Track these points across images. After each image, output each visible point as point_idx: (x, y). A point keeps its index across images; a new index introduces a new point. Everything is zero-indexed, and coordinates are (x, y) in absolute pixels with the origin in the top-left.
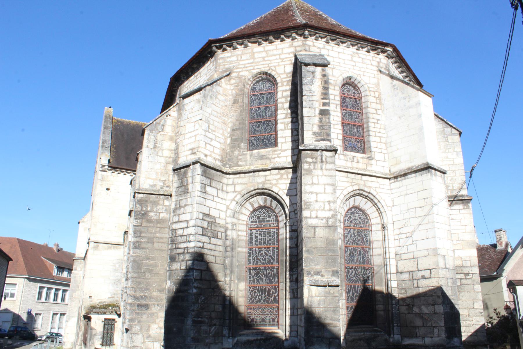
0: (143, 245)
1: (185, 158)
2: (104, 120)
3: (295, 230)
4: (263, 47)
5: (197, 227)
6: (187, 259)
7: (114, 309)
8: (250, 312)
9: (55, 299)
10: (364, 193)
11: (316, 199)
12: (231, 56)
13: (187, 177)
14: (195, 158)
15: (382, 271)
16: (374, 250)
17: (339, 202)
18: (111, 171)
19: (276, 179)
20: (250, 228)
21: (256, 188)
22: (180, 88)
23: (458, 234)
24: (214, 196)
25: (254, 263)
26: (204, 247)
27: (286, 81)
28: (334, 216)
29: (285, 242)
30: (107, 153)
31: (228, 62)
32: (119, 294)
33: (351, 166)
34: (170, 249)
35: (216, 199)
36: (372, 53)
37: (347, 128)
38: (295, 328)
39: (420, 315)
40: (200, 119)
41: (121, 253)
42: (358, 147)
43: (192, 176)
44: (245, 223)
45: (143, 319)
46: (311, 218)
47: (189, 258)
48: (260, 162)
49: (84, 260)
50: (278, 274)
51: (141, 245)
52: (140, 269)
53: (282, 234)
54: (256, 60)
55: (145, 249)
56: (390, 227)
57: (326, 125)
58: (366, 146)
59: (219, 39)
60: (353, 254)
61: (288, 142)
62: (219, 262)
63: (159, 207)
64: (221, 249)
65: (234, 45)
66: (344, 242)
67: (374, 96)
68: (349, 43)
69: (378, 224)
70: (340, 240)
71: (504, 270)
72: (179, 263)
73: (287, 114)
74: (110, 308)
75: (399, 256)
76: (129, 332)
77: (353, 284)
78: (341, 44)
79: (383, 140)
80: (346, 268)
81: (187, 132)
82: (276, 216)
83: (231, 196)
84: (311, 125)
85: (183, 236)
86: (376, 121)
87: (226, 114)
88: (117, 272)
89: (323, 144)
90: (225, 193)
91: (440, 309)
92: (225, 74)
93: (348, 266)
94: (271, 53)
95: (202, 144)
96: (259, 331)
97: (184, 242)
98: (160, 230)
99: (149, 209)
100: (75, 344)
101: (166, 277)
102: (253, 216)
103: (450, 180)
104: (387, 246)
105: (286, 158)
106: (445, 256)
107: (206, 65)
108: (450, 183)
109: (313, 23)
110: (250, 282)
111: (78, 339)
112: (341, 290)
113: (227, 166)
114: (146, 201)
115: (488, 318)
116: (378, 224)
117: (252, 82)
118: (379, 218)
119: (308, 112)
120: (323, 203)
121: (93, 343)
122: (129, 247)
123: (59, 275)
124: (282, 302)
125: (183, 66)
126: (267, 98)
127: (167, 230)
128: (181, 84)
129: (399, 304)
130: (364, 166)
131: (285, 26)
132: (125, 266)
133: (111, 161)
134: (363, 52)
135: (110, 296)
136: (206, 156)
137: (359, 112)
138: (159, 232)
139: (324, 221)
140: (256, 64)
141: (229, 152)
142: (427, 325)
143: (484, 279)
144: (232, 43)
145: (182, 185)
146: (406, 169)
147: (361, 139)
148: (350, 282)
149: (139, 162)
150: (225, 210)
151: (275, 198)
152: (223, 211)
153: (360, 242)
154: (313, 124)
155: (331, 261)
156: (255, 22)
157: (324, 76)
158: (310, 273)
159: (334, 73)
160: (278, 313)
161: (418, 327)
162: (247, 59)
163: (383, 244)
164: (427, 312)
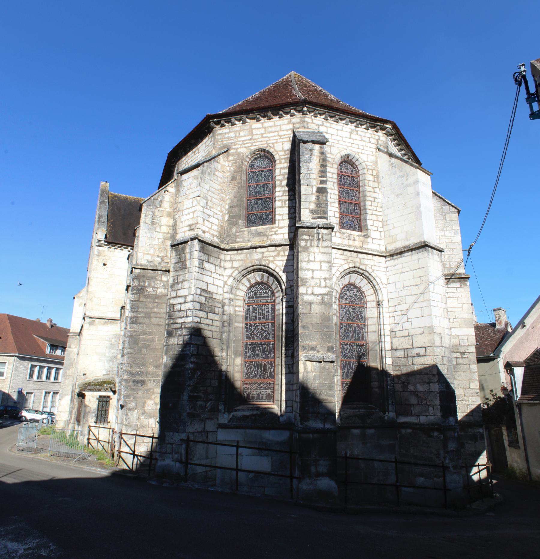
0: (140, 320)
2: (100, 195)
4: (261, 123)
6: (184, 334)
7: (109, 386)
8: (246, 388)
9: (48, 377)
10: (360, 271)
11: (312, 276)
12: (230, 132)
13: (185, 253)
14: (193, 234)
15: (377, 348)
16: (369, 327)
17: (334, 279)
18: (108, 247)
19: (273, 256)
20: (248, 303)
21: (254, 264)
22: (177, 163)
24: (211, 272)
25: (250, 338)
26: (202, 322)
28: (329, 293)
29: (281, 318)
31: (226, 138)
32: (115, 371)
33: (347, 244)
34: (167, 324)
35: (214, 275)
36: (371, 131)
37: (344, 206)
38: (290, 404)
39: (415, 394)
40: (198, 195)
41: (117, 328)
42: (354, 225)
43: (190, 252)
44: (242, 298)
46: (307, 294)
47: (186, 333)
48: (257, 238)
49: (79, 335)
50: (274, 349)
51: (138, 320)
52: (137, 344)
53: (279, 310)
54: (255, 137)
55: (143, 324)
56: (385, 304)
57: (323, 203)
58: (362, 224)
59: (217, 114)
60: (348, 330)
62: (216, 337)
63: (156, 282)
64: (219, 324)
65: (232, 121)
66: (339, 319)
67: (372, 174)
68: (348, 120)
69: (374, 301)
71: (501, 351)
72: (176, 338)
73: (284, 191)
74: (105, 385)
75: (394, 333)
76: (124, 408)
77: (348, 360)
78: (339, 121)
79: (380, 218)
80: (341, 344)
81: (185, 208)
82: (273, 292)
83: (228, 272)
85: (180, 311)
86: (372, 199)
87: (223, 191)
88: (113, 349)
89: (320, 222)
90: (223, 269)
91: (435, 387)
92: (223, 151)
93: (343, 342)
94: (270, 130)
95: (200, 221)
96: (255, 406)
97: (181, 317)
98: (157, 305)
99: (146, 284)
100: (68, 422)
101: (163, 353)
102: (250, 292)
103: (448, 258)
104: (382, 323)
105: (283, 235)
106: (441, 334)
107: (204, 141)
108: (447, 261)
109: (312, 99)
110: (246, 357)
111: (71, 418)
112: (336, 366)
113: (225, 242)
114: (144, 276)
115: (484, 399)
116: (374, 301)
117: (250, 159)
118: (374, 295)
119: (306, 190)
120: (319, 280)
121: (87, 421)
122: (126, 322)
123: (52, 353)
124: (278, 377)
125: (181, 142)
126: (265, 175)
127: (165, 305)
128: (179, 160)
131: (284, 102)
132: (121, 341)
133: (108, 236)
134: (362, 129)
135: (105, 373)
136: (204, 232)
137: (356, 191)
138: (157, 307)
139: (320, 298)
140: (254, 141)
141: (227, 228)
143: (480, 360)
144: (231, 119)
145: (179, 261)
146: (402, 248)
147: (357, 217)
149: (136, 238)
150: (222, 286)
151: (272, 275)
152: (220, 287)
154: (310, 202)
155: (326, 337)
156: (253, 97)
157: (322, 153)
159: (332, 151)
160: (274, 388)
162: (245, 136)
163: (378, 321)
164: (422, 390)
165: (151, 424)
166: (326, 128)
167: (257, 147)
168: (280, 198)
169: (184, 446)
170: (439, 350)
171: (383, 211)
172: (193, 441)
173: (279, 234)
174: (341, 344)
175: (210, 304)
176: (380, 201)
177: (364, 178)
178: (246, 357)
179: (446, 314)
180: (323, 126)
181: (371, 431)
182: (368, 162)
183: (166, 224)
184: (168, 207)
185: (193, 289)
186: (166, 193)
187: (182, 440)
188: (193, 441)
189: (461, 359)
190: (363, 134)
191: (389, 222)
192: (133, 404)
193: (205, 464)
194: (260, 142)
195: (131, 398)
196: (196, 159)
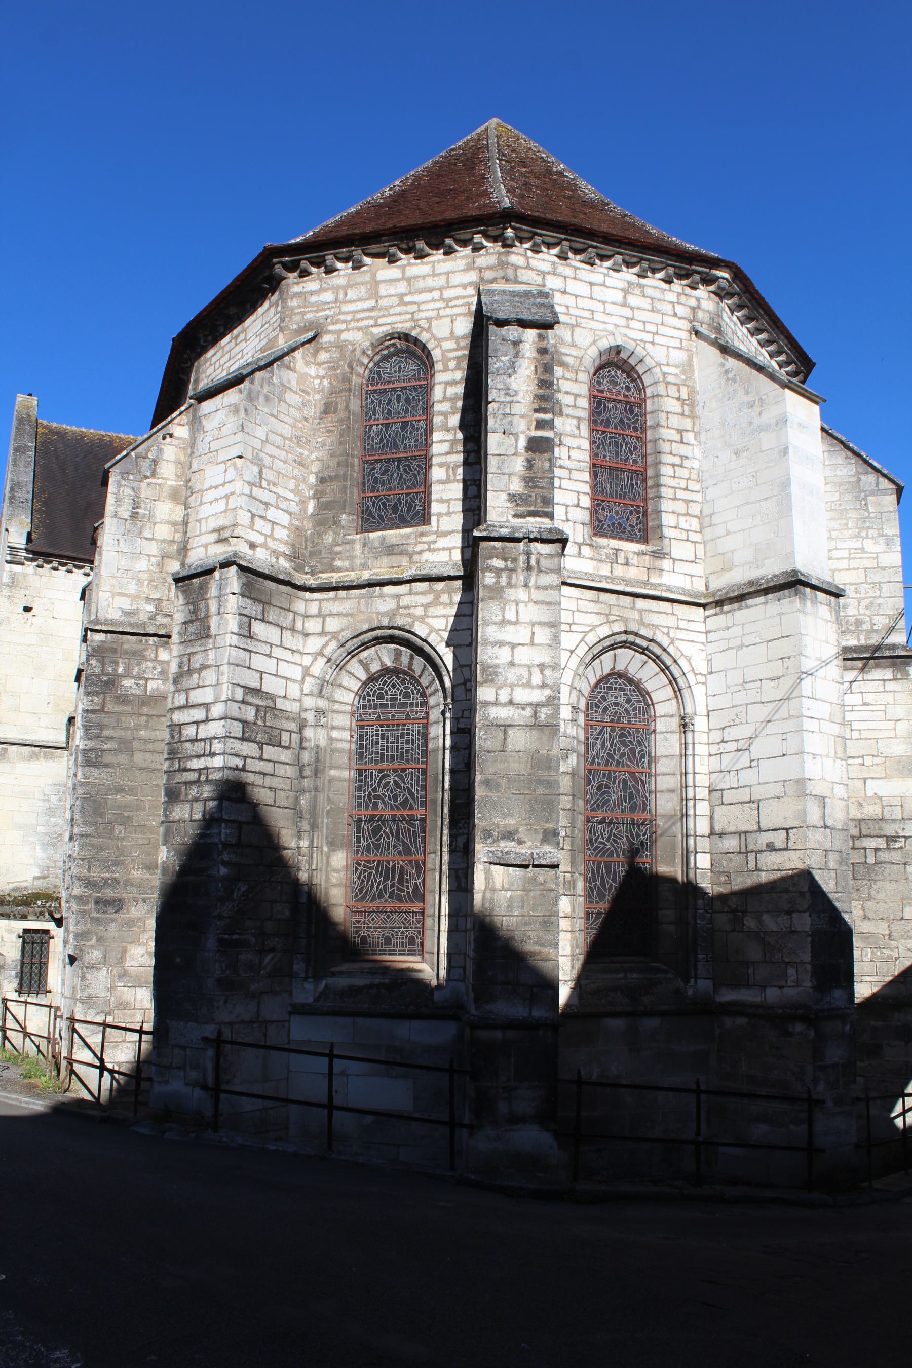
0: (108, 758)
1: (202, 550)
2: (14, 430)
3: (464, 729)
5: (229, 721)
6: (205, 795)
7: (48, 905)
10: (639, 641)
11: (510, 659)
12: (321, 290)
13: (207, 600)
15: (677, 829)
16: (658, 778)
18: (35, 564)
19: (422, 606)
20: (361, 720)
21: (375, 625)
22: (196, 364)
23: (877, 740)
24: (271, 645)
27: (455, 358)
29: (441, 757)
30: (23, 517)
31: (312, 305)
33: (609, 574)
34: (166, 772)
35: (277, 652)
36: (678, 285)
37: (604, 477)
42: (630, 526)
43: (219, 597)
44: (348, 708)
45: (110, 934)
46: (496, 703)
47: (210, 795)
48: (385, 561)
51: (101, 757)
52: (101, 815)
55: (113, 767)
56: (700, 724)
57: (543, 478)
58: (650, 524)
60: (607, 787)
61: (454, 512)
62: (284, 803)
63: (144, 665)
64: (290, 771)
66: (586, 760)
67: (677, 395)
68: (619, 258)
69: (672, 716)
70: (575, 755)
74: (39, 903)
75: (718, 794)
76: (76, 963)
77: (605, 858)
79: (695, 509)
80: (588, 821)
81: (206, 486)
82: (423, 695)
83: (314, 644)
84: (506, 477)
85: (196, 740)
86: (677, 460)
88: (54, 816)
89: (533, 524)
90: (301, 637)
91: (804, 922)
93: (593, 817)
94: (421, 284)
95: (244, 518)
96: (377, 965)
97: (199, 757)
98: (147, 721)
99: (120, 670)
103: (867, 608)
104: (690, 770)
106: (824, 798)
107: (260, 310)
108: (864, 614)
110: (358, 851)
114: (115, 651)
116: (672, 716)
117: (371, 360)
118: (674, 702)
119: (500, 445)
120: (526, 669)
124: (431, 898)
126: (408, 401)
128: (199, 355)
129: (712, 909)
130: (642, 575)
134: (654, 282)
135: (39, 875)
136: (253, 546)
137: (638, 438)
138: (146, 727)
139: (528, 712)
141: (312, 535)
142: (773, 960)
146: (745, 584)
147: (638, 506)
148: (596, 855)
151: (419, 651)
152: (294, 681)
153: (625, 759)
154: (510, 475)
156: (387, 193)
157: (543, 351)
158: (490, 836)
159: (575, 338)
160: (423, 924)
161: (753, 962)
162: (359, 300)
163: (681, 766)
164: (775, 929)
165: (142, 1001)
166: (561, 279)
167: (386, 329)
168: (443, 459)
169: (210, 1053)
170: (817, 837)
171: (703, 491)
172: (232, 1043)
173: (438, 549)
174: (588, 821)
175: (267, 724)
176: (696, 465)
177: (656, 407)
178: (358, 851)
179: (840, 750)
180: (554, 274)
181: (650, 1023)
182: (668, 365)
183: (167, 518)
184: (172, 477)
185: (225, 687)
186: (168, 439)
187: (205, 1039)
188: (232, 1043)
189: (886, 852)
190: (657, 294)
191: (715, 520)
192: (97, 954)
193: (261, 1094)
194: (395, 314)
195: (92, 939)
196: (240, 355)
